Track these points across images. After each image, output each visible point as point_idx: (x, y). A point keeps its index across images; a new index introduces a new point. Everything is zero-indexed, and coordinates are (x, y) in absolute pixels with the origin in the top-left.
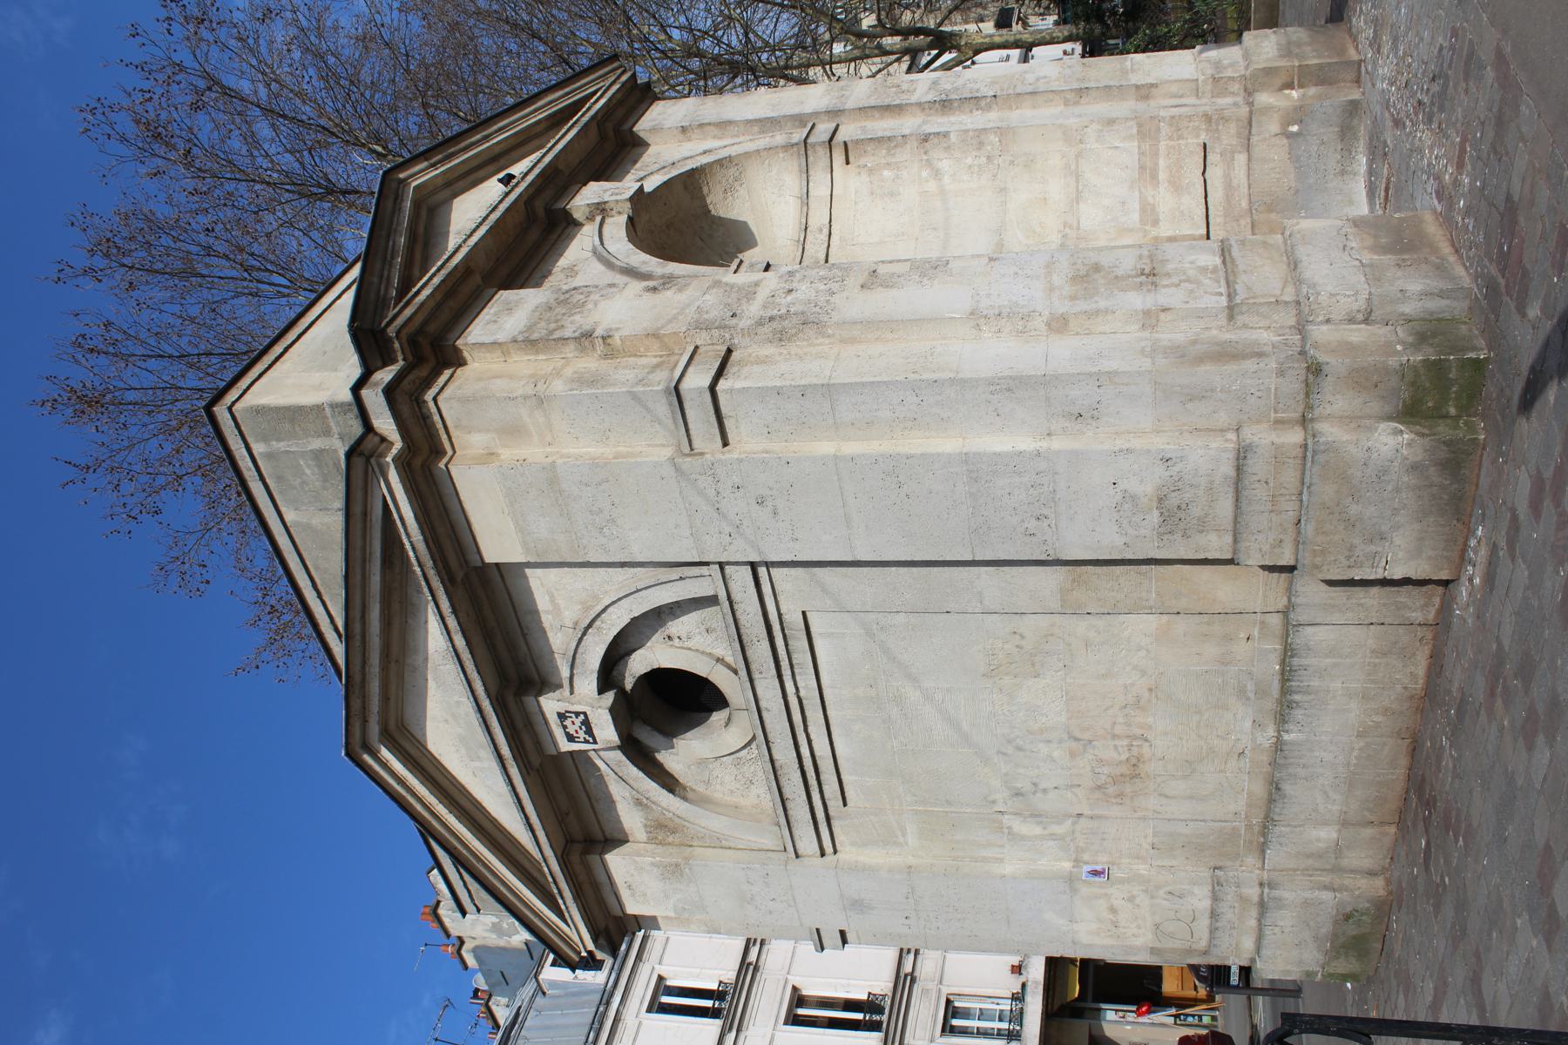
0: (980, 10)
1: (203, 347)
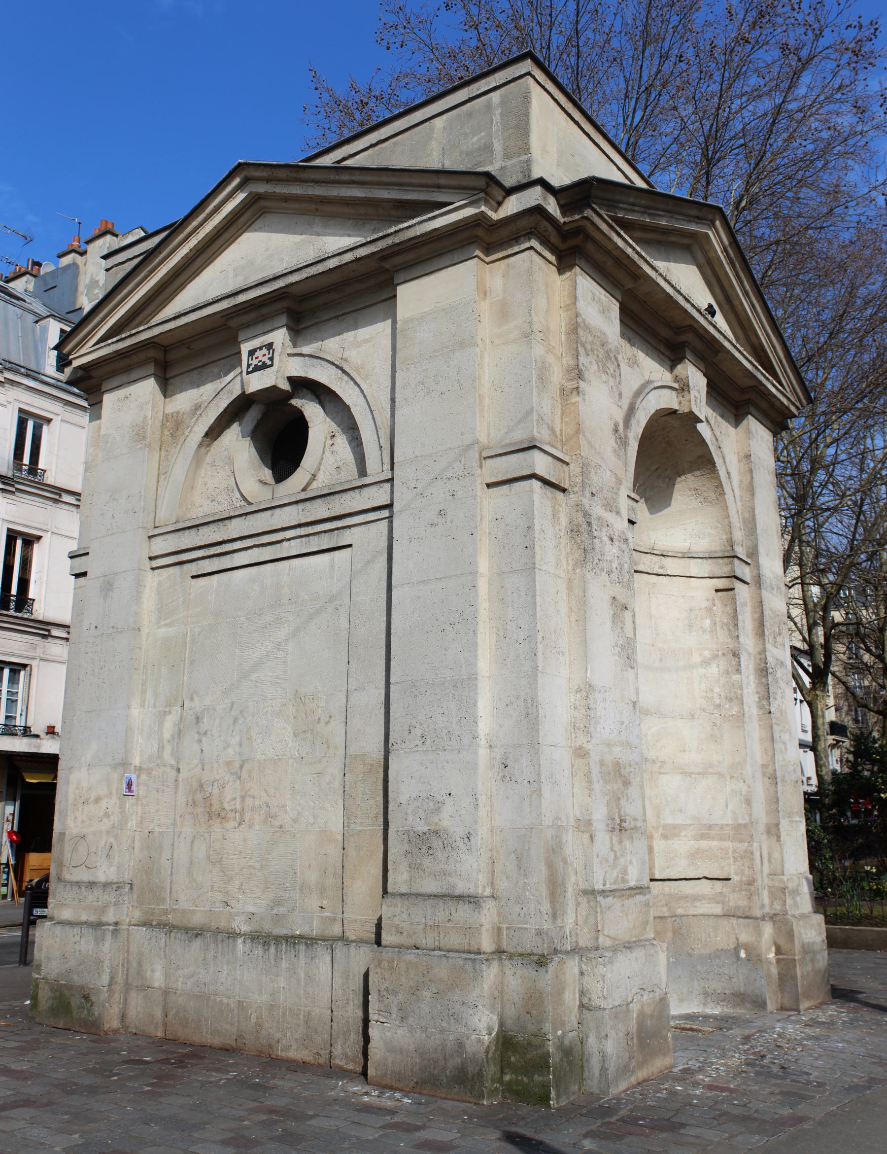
0: (845, 708)
1: (584, 50)
